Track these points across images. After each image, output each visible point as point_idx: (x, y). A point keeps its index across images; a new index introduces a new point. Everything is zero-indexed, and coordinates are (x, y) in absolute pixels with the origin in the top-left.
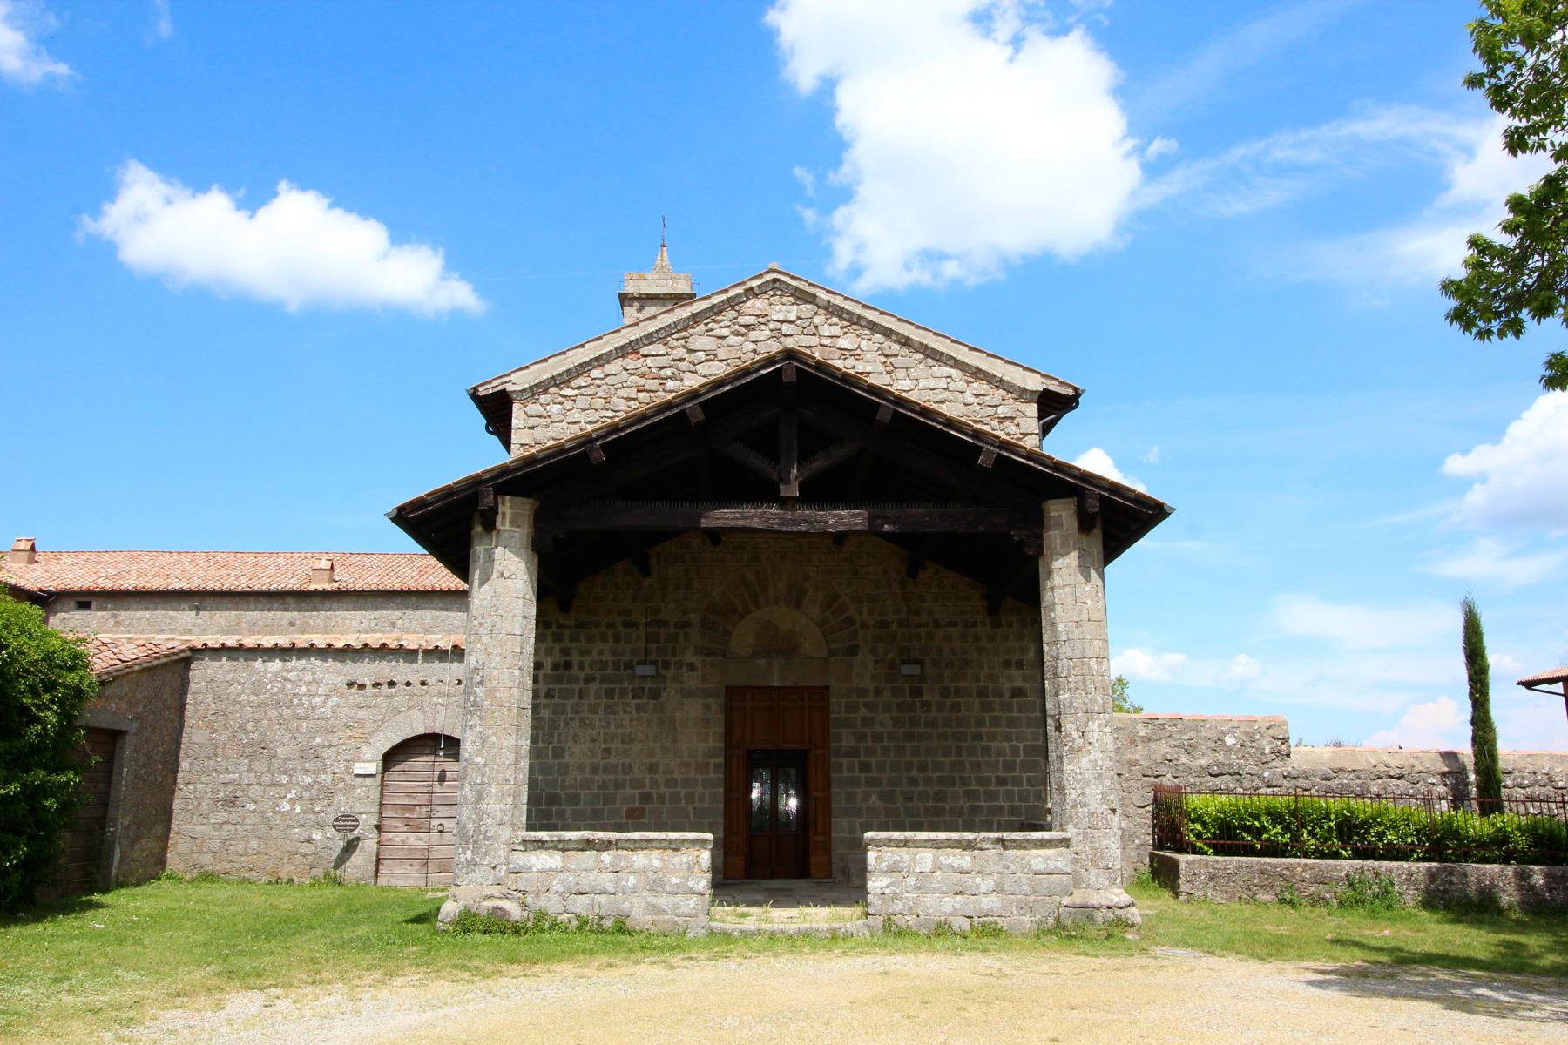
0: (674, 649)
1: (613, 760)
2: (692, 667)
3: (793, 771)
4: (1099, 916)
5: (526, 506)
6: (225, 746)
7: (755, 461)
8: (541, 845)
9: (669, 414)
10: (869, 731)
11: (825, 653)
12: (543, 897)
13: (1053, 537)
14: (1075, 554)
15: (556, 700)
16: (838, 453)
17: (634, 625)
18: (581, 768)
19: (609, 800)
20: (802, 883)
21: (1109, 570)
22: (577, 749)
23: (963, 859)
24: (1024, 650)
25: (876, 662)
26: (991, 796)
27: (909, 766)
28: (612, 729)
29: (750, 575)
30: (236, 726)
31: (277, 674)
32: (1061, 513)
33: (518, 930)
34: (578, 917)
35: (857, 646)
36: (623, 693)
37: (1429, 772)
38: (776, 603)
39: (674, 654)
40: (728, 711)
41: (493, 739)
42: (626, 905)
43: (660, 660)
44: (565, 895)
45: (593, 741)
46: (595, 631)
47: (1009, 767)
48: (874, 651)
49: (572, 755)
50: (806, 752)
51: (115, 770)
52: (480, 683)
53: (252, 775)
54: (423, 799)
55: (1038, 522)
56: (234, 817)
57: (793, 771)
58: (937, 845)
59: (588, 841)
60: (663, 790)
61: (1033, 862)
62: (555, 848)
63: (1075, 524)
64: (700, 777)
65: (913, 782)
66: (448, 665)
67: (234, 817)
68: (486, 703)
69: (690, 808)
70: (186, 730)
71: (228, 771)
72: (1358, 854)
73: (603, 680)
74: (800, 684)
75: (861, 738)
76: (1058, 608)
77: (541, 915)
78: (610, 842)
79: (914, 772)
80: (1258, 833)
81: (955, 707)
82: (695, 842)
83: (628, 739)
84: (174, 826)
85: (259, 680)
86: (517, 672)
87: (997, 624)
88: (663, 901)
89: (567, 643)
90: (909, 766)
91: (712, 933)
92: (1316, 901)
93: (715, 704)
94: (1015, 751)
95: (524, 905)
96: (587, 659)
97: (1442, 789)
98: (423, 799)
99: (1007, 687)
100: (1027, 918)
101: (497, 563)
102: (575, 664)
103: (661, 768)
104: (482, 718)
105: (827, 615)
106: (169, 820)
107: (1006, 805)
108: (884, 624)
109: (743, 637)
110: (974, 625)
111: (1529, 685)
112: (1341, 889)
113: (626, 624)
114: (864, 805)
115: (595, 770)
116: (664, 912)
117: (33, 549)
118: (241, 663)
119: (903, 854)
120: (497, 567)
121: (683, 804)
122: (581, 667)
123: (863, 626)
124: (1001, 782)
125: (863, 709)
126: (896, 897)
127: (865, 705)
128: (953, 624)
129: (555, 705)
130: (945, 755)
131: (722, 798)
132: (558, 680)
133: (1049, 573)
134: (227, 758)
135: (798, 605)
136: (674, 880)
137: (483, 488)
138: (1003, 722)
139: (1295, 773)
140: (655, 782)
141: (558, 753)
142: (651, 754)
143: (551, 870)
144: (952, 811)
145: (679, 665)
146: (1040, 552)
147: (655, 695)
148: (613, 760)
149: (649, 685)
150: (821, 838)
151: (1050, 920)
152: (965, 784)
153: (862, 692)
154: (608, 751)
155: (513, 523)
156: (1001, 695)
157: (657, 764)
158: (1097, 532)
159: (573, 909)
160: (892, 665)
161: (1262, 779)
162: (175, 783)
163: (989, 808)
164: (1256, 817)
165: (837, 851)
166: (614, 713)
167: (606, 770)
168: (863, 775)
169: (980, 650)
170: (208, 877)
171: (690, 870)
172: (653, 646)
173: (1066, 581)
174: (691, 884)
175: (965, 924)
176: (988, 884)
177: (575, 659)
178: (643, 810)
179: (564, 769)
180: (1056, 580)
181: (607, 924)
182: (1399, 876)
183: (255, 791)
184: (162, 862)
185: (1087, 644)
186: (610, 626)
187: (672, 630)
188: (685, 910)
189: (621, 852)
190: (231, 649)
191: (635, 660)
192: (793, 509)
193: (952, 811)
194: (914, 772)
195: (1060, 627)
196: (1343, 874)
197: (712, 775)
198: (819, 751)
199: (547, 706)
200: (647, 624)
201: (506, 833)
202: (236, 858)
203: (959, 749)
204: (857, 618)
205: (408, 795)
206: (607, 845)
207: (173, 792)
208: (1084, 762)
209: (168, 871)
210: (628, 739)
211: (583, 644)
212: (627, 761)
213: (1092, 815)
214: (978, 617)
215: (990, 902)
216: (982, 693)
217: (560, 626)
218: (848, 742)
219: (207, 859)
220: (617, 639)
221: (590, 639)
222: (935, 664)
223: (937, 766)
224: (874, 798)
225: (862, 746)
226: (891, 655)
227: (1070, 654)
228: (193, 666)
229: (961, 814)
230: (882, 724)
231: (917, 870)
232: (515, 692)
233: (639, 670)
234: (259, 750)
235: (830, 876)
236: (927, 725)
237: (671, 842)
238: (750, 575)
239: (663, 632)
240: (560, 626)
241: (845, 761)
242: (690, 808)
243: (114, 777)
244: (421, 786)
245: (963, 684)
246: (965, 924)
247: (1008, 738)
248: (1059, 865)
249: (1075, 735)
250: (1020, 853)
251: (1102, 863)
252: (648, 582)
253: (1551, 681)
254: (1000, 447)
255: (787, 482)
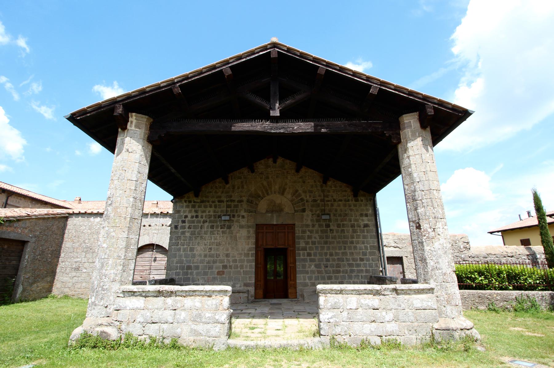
0: (237, 210)
1: (212, 252)
2: (243, 217)
3: (282, 257)
4: (456, 335)
5: (144, 120)
6: (77, 248)
7: (258, 100)
8: (133, 293)
9: (214, 71)
10: (310, 241)
11: (293, 212)
12: (131, 325)
13: (406, 133)
14: (420, 139)
15: (192, 230)
16: (298, 97)
17: (223, 201)
18: (200, 255)
19: (211, 268)
20: (284, 301)
21: (434, 148)
22: (199, 248)
23: (374, 301)
24: (368, 210)
25: (312, 215)
26: (358, 265)
27: (326, 254)
28: (213, 241)
29: (265, 183)
30: (82, 241)
31: (98, 223)
32: (410, 121)
33: (116, 345)
34: (150, 337)
35: (305, 209)
36: (217, 227)
37: (522, 254)
38: (275, 193)
39: (237, 212)
40: (257, 233)
41: (113, 234)
42: (179, 330)
43: (231, 214)
44: (144, 324)
45: (205, 245)
46: (207, 204)
47: (365, 254)
48: (311, 211)
49: (197, 250)
50: (286, 249)
51: (23, 256)
52: (110, 205)
53: (86, 259)
54: (147, 268)
55: (397, 127)
56: (78, 274)
57: (282, 257)
58: (359, 293)
59: (159, 291)
60: (231, 264)
61: (414, 302)
62: (141, 295)
63: (418, 125)
64: (245, 258)
65: (328, 260)
66: (159, 219)
67: (78, 274)
68: (112, 215)
69: (242, 271)
70: (64, 242)
71: (77, 257)
72: (515, 288)
73: (210, 222)
74: (284, 223)
75: (307, 243)
76: (413, 166)
77: (129, 336)
78: (172, 292)
79: (328, 256)
80: (473, 280)
81: (343, 231)
82: (220, 291)
83: (219, 244)
84: (56, 278)
85: (92, 225)
86: (132, 199)
87: (357, 200)
88: (200, 328)
89: (197, 208)
90: (326, 254)
91: (229, 348)
92: (505, 309)
93: (252, 231)
94: (366, 248)
95: (120, 330)
96: (204, 214)
97: (527, 261)
98: (147, 268)
99: (362, 223)
100: (414, 337)
101: (125, 145)
102: (200, 216)
103: (231, 255)
104: (109, 223)
105: (294, 197)
106: (55, 275)
107: (364, 269)
108: (315, 201)
109: (263, 205)
110: (348, 201)
111: (491, 233)
112: (514, 304)
113: (219, 201)
114: (309, 269)
115: (205, 256)
116: (201, 334)
117: (80, 200)
118: (86, 219)
119: (340, 298)
120: (126, 147)
121: (239, 269)
122: (202, 217)
123: (307, 201)
124: (362, 260)
125: (308, 232)
126: (336, 325)
127: (309, 231)
128: (341, 201)
129: (192, 231)
130: (339, 250)
131: (254, 266)
132: (193, 222)
133: (406, 150)
134: (77, 253)
135: (283, 194)
136: (208, 315)
137: (117, 105)
138: (361, 237)
139: (473, 256)
140: (228, 261)
141: (192, 250)
142: (227, 250)
143: (137, 308)
144: (343, 272)
145: (239, 216)
146: (399, 141)
147: (229, 227)
148: (212, 252)
149: (227, 223)
150: (293, 283)
151: (427, 337)
152: (348, 261)
153: (307, 226)
154: (211, 249)
155: (136, 126)
156: (360, 227)
157: (229, 254)
158: (428, 129)
159: (147, 332)
160: (318, 216)
161: (461, 258)
162: (58, 261)
163: (357, 270)
164: (471, 273)
165: (299, 288)
166: (213, 234)
167: (210, 256)
168: (308, 258)
169: (351, 210)
170: (66, 297)
171: (217, 309)
172: (229, 209)
173: (415, 151)
174: (217, 317)
175: (378, 341)
176: (389, 316)
177: (200, 214)
178: (224, 272)
179: (194, 256)
180: (410, 152)
181: (167, 341)
182: (538, 297)
183: (86, 265)
184: (50, 290)
185: (431, 183)
186: (213, 202)
187: (236, 203)
188: (213, 333)
189: (178, 298)
190: (83, 214)
191: (222, 214)
192: (277, 122)
193: (343, 272)
194: (328, 256)
195: (415, 175)
196: (514, 297)
197: (250, 258)
198: (291, 249)
199: (189, 232)
200: (227, 201)
201: (116, 287)
202: (77, 290)
203: (345, 247)
204: (305, 198)
205: (142, 266)
206: (171, 294)
207: (57, 265)
208: (437, 245)
209: (53, 294)
210: (219, 244)
211: (203, 209)
212: (218, 253)
213: (445, 274)
214: (350, 198)
215: (392, 327)
216: (353, 226)
217: (194, 202)
218: (302, 245)
219: (66, 290)
220: (215, 207)
221: (206, 207)
222: (335, 215)
223: (337, 254)
224: (313, 266)
225: (308, 246)
226: (318, 212)
227: (422, 188)
228: (69, 220)
229: (347, 273)
230: (315, 238)
231: (348, 308)
232: (129, 210)
233: (223, 218)
234: (89, 250)
235: (296, 298)
236: (332, 238)
237: (206, 292)
238: (265, 183)
239: (233, 204)
240: (194, 202)
241: (301, 252)
242: (242, 271)
243: (22, 259)
244: (147, 263)
245: (345, 223)
246: (378, 341)
247: (363, 243)
248: (429, 304)
249: (429, 230)
250: (407, 297)
251: (453, 303)
252: (227, 186)
253: (498, 232)
254: (380, 85)
255: (274, 109)
